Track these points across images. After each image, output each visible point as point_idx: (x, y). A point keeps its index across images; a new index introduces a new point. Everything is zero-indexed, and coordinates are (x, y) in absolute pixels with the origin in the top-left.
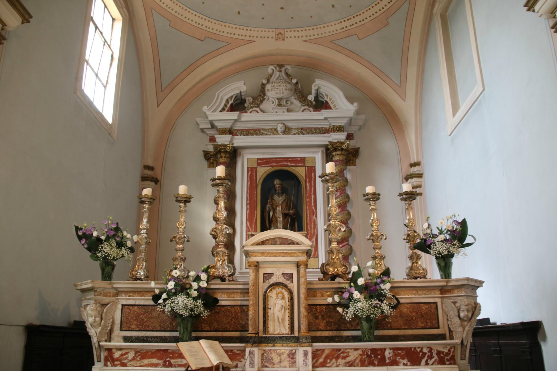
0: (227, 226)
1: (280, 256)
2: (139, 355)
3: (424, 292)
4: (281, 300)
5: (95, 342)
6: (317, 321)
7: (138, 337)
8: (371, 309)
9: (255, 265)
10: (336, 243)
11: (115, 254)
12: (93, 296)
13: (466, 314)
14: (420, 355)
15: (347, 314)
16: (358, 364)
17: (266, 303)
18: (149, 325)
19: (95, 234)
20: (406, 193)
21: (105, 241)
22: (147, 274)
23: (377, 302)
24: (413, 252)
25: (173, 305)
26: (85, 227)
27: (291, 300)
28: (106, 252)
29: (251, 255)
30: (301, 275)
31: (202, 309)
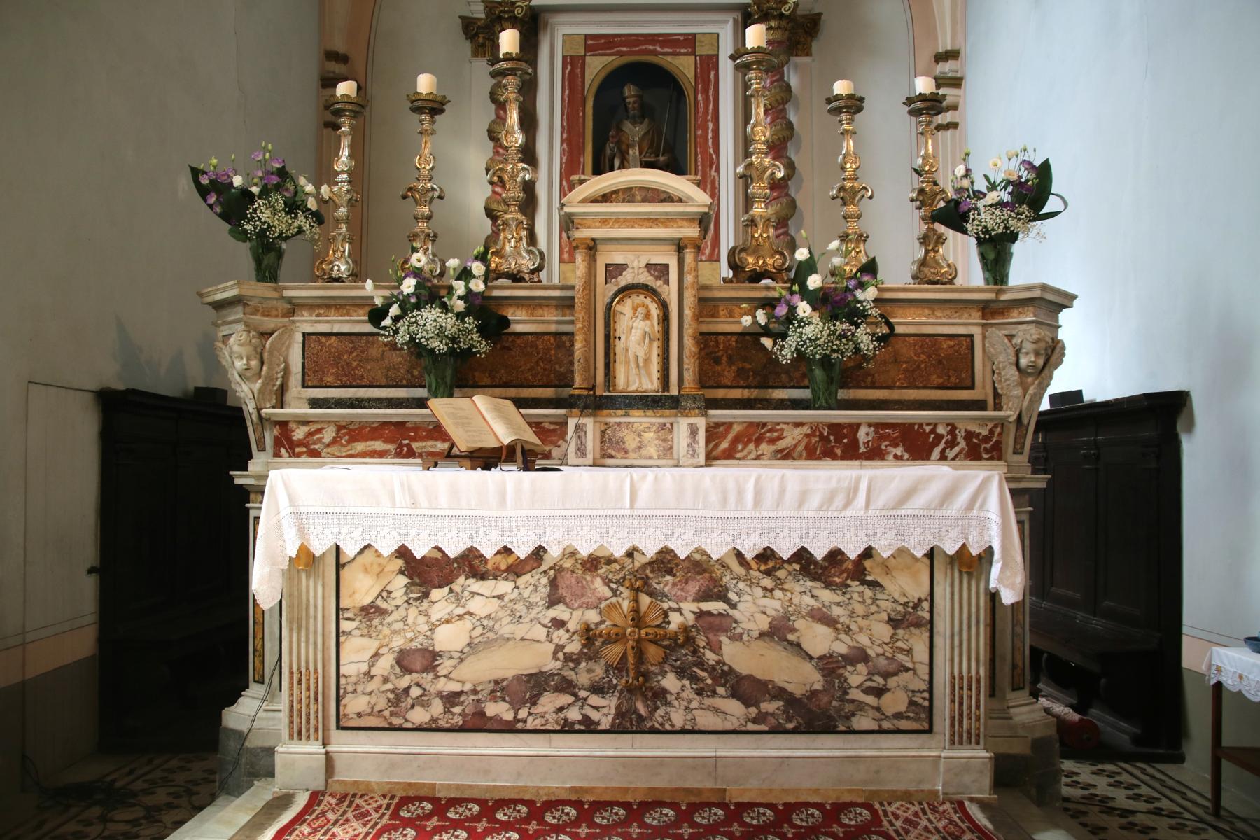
0: (525, 166)
1: (641, 226)
2: (345, 435)
3: (948, 312)
4: (643, 320)
5: (251, 411)
6: (719, 368)
7: (340, 399)
8: (832, 342)
9: (588, 246)
10: (763, 205)
11: (284, 226)
12: (240, 315)
13: (1033, 359)
14: (931, 440)
15: (781, 350)
16: (801, 453)
17: (612, 326)
18: (362, 376)
19: (238, 181)
20: (922, 97)
21: (260, 198)
22: (353, 270)
23: (846, 326)
24: (928, 229)
25: (413, 328)
26: (215, 167)
27: (663, 321)
28: (263, 220)
29: (579, 224)
30: (686, 268)
31: (476, 336)
